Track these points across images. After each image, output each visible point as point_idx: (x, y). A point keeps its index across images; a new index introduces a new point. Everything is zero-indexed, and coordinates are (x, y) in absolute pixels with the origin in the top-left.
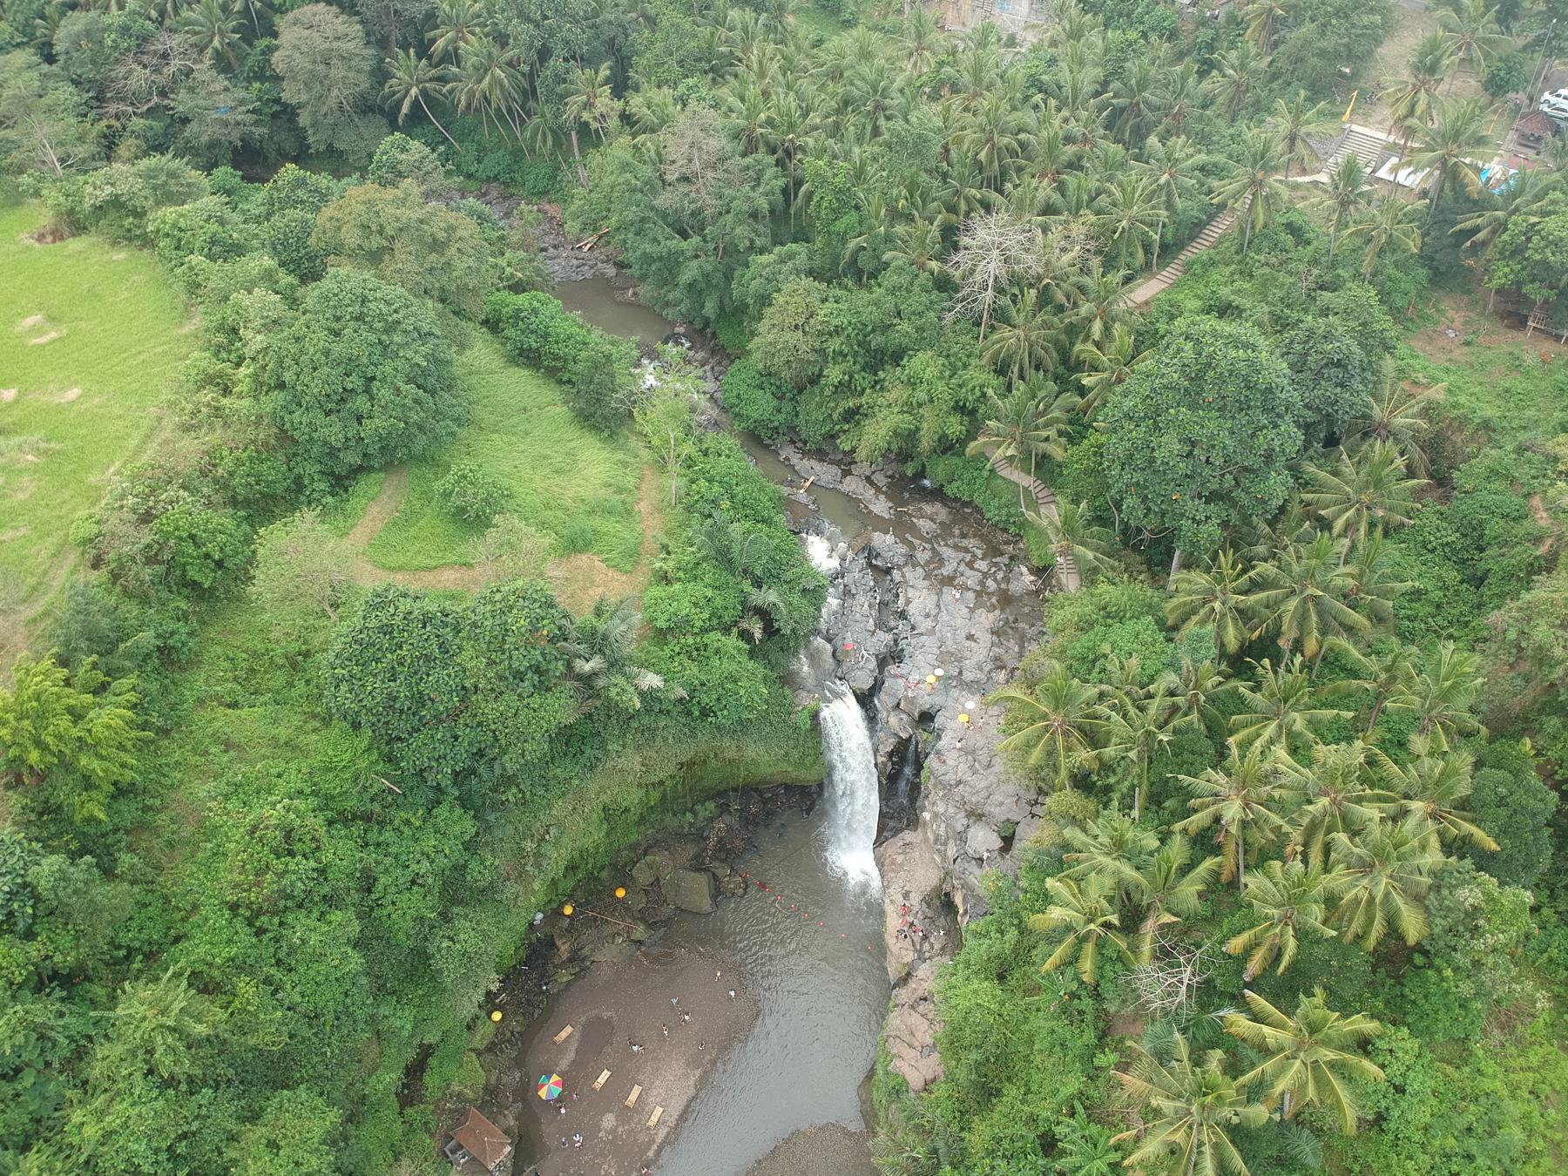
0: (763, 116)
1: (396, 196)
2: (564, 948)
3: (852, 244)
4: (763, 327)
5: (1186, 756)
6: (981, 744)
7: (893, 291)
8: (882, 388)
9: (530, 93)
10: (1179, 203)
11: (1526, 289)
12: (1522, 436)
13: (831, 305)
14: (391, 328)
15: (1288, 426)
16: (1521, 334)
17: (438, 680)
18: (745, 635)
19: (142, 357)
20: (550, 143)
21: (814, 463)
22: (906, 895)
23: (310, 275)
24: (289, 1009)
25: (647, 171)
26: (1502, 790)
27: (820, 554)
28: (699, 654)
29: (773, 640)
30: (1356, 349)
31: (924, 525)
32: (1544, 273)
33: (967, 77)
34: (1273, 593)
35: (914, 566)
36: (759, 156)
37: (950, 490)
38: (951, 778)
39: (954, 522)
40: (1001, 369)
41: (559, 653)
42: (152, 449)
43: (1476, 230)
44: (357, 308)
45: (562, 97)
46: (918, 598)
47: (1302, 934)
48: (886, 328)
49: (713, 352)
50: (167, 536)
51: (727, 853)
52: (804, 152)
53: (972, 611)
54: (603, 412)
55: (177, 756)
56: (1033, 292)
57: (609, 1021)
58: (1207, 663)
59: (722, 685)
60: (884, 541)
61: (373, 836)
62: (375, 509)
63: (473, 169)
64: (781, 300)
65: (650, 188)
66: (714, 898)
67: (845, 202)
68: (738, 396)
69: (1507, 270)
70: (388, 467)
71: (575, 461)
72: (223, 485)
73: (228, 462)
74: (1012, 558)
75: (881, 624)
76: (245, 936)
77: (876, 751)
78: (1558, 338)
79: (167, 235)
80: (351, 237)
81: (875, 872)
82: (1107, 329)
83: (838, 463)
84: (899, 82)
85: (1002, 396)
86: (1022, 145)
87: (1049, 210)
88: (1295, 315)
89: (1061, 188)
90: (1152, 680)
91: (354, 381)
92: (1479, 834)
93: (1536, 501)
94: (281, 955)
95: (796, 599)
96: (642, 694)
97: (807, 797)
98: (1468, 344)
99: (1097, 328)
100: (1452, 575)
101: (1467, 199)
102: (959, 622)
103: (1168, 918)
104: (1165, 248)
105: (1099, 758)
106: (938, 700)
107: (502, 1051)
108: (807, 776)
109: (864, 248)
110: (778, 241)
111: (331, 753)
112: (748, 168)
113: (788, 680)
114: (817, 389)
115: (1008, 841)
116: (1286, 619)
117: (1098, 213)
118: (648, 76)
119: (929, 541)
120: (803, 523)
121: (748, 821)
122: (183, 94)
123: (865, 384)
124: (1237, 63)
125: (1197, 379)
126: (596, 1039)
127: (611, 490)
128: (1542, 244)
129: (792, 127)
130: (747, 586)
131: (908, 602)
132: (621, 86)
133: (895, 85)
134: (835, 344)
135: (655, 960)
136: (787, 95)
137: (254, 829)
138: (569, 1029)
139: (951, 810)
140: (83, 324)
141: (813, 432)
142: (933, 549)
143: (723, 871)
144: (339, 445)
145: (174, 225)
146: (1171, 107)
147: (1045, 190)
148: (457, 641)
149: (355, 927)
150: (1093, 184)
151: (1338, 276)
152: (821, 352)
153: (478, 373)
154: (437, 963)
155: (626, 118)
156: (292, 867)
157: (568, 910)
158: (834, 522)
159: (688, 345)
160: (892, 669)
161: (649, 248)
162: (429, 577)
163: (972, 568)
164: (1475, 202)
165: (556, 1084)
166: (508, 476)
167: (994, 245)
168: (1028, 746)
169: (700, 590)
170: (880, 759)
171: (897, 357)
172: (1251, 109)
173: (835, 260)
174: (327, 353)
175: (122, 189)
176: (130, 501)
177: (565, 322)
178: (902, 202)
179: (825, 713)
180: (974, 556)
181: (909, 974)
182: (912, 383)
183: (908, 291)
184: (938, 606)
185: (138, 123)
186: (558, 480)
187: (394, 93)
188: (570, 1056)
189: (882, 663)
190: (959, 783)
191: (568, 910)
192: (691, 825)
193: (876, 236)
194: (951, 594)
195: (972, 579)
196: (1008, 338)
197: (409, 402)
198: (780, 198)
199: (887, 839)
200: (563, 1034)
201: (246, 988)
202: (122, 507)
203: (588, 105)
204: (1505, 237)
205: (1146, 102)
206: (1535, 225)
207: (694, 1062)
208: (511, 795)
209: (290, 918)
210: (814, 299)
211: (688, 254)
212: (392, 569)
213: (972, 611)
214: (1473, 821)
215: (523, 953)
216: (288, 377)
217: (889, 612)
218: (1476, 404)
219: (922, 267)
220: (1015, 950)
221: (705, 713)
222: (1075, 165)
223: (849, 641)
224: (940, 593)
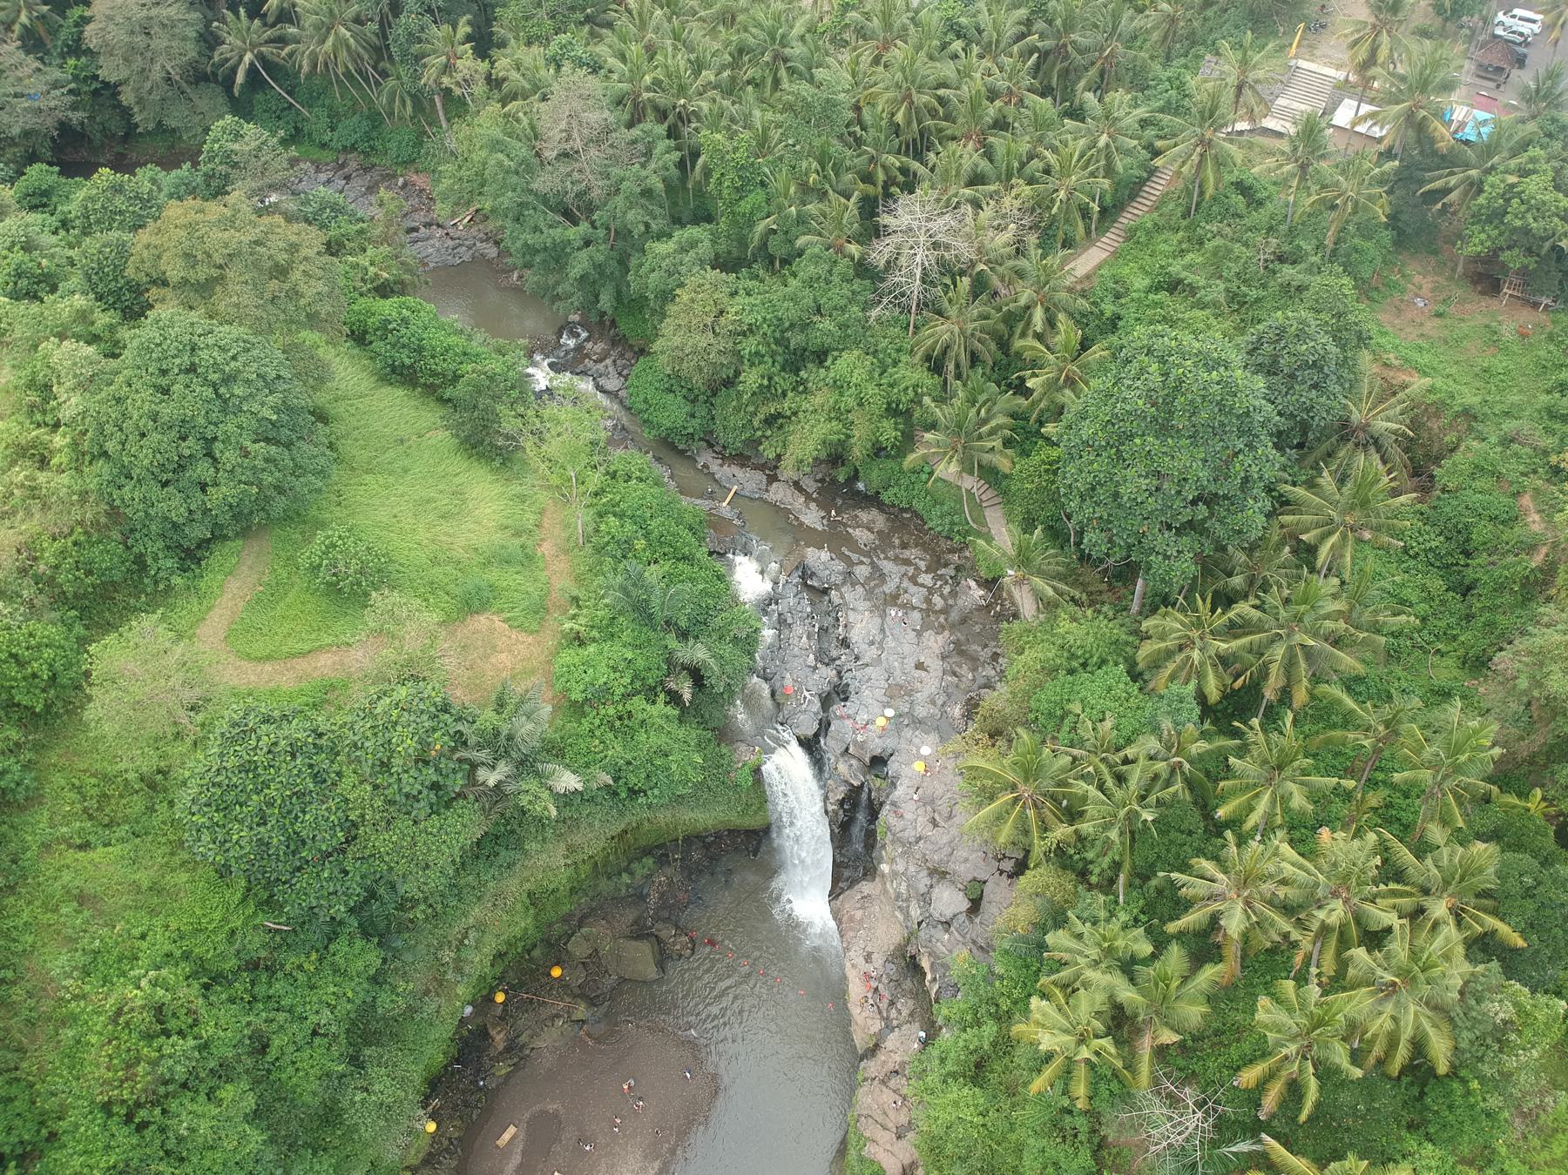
0: (648, 79)
1: (229, 213)
2: (499, 1038)
3: (760, 227)
4: (667, 327)
5: (1173, 835)
6: (939, 792)
7: (810, 283)
9: (380, 51)
10: (1119, 166)
11: (1505, 256)
12: (1509, 426)
13: (741, 299)
14: (229, 379)
15: (1266, 448)
16: (1495, 302)
17: (317, 820)
18: (674, 698)
20: (409, 108)
21: (735, 470)
22: (868, 958)
23: (134, 312)
25: (521, 150)
26: (1528, 880)
28: (624, 725)
29: (702, 701)
30: (1333, 349)
31: (861, 535)
32: (1526, 240)
33: (876, 22)
35: (853, 585)
36: (647, 126)
37: (886, 497)
38: (910, 834)
39: (893, 530)
40: (935, 364)
41: (457, 762)
43: (1447, 191)
44: (186, 359)
45: (418, 58)
46: (861, 624)
47: (1326, 1073)
48: (805, 326)
49: (614, 343)
53: (919, 634)
55: (25, 916)
56: (966, 280)
57: (556, 1116)
58: (1190, 726)
60: (818, 558)
61: (261, 990)
62: (234, 585)
64: (685, 298)
65: (526, 169)
67: (749, 180)
68: (646, 401)
69: (1483, 236)
70: (245, 533)
71: (464, 501)
72: (46, 583)
73: (49, 556)
74: (958, 569)
75: (824, 658)
76: (124, 1137)
77: (826, 798)
78: (1536, 305)
80: (174, 273)
81: (832, 924)
82: (1051, 322)
83: (761, 467)
84: (799, 28)
85: (940, 400)
87: (976, 179)
88: (1254, 293)
89: (989, 155)
91: (191, 446)
92: (1503, 929)
93: (1526, 501)
95: (727, 650)
96: (557, 797)
97: (752, 843)
98: (1439, 315)
99: (1038, 316)
100: (1437, 584)
101: (1435, 153)
102: (907, 649)
103: (1169, 1037)
104: (1104, 211)
105: (1076, 831)
106: (890, 743)
107: (440, 1163)
109: (774, 232)
110: (678, 221)
111: (198, 912)
112: (634, 142)
113: (724, 734)
114: (732, 392)
115: (975, 906)
117: (1031, 181)
118: (515, 30)
120: (723, 542)
125: (1167, 407)
127: (508, 533)
128: (1523, 208)
129: (682, 90)
130: (672, 642)
132: (484, 44)
134: (750, 345)
137: (119, 1013)
138: (512, 1130)
139: (912, 869)
142: (872, 563)
144: (181, 520)
146: (1102, 50)
147: (968, 156)
149: (250, 1102)
150: (1024, 147)
151: (1299, 248)
152: (738, 354)
154: (350, 1118)
155: (494, 82)
156: (167, 1050)
157: (500, 998)
158: (764, 538)
159: (584, 335)
160: (838, 709)
161: (530, 239)
162: (302, 665)
163: (916, 584)
164: (1443, 157)
167: (918, 227)
168: (999, 818)
169: (618, 651)
170: (830, 808)
171: (821, 356)
172: (1186, 43)
173: (743, 242)
174: (155, 417)
177: (442, 324)
180: (917, 568)
181: (877, 1046)
182: (839, 386)
183: (828, 282)
184: (882, 630)
186: (445, 526)
187: (227, 60)
188: (516, 1159)
189: (826, 701)
191: (500, 998)
193: (787, 217)
195: (916, 596)
196: (942, 332)
197: (259, 463)
198: (674, 172)
199: (843, 891)
200: (507, 1136)
203: (447, 69)
204: (1481, 200)
205: (1073, 42)
206: (1513, 186)
207: (651, 1153)
208: (419, 913)
209: (173, 1106)
210: (721, 295)
211: (576, 245)
212: (259, 660)
213: (919, 634)
214: (1494, 913)
215: (454, 1051)
216: (111, 446)
217: (831, 642)
218: (1453, 387)
219: (840, 250)
221: (633, 793)
222: (1001, 125)
223: (788, 682)
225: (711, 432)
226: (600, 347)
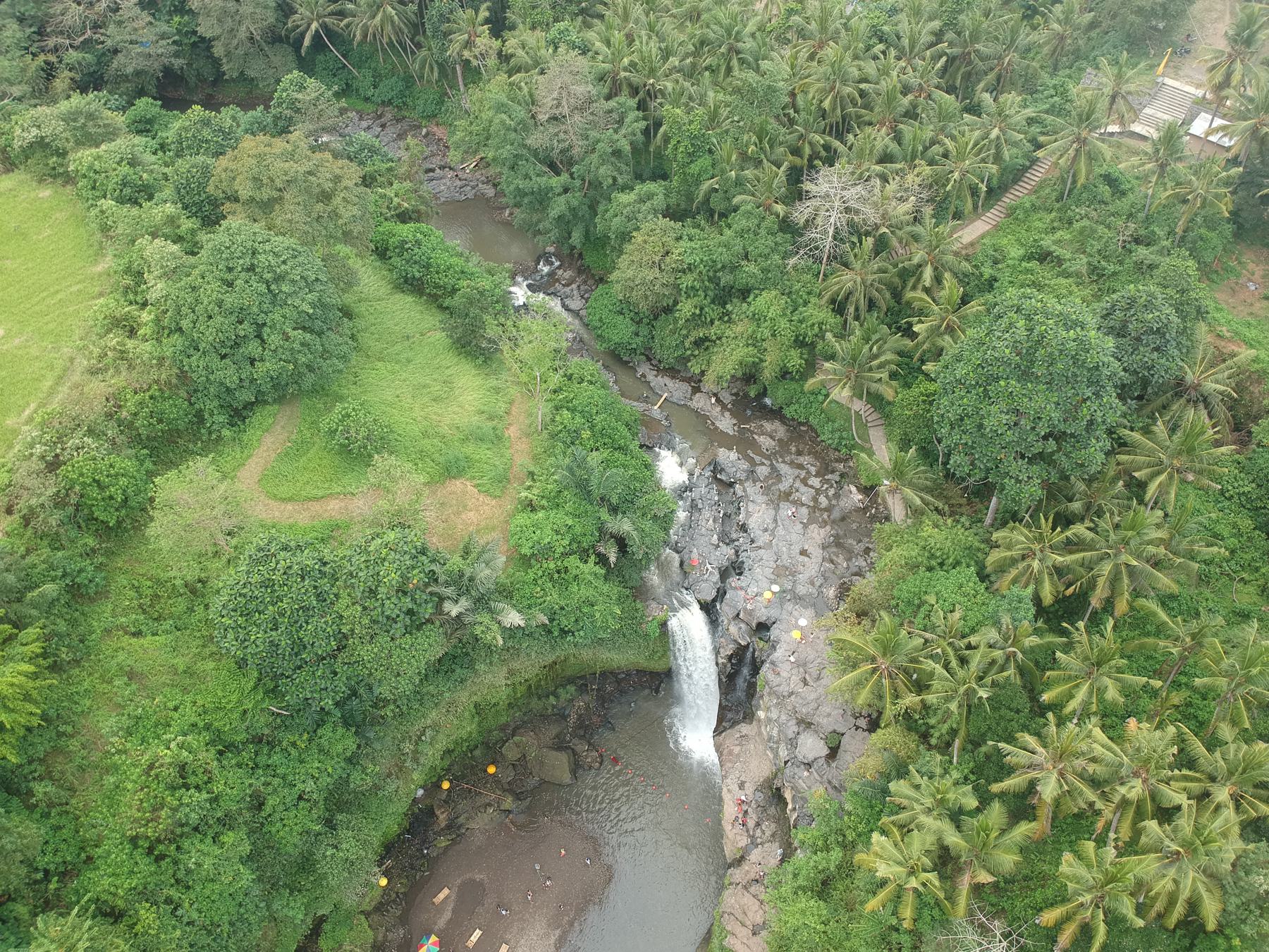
0: (626, 61)
2: (442, 817)
3: (705, 186)
4: (623, 262)
5: (1003, 711)
7: (741, 234)
8: (729, 321)
13: (684, 244)
14: (279, 278)
17: (317, 630)
18: (602, 560)
19: (59, 297)
20: (436, 74)
21: (667, 380)
23: (211, 220)
24: (188, 924)
25: (520, 113)
27: (671, 469)
28: (561, 578)
29: (624, 564)
30: (1175, 319)
31: (765, 442)
33: (814, 26)
34: (1088, 554)
36: (622, 99)
37: (788, 412)
38: (784, 689)
39: (791, 440)
40: (838, 306)
41: (429, 594)
42: (64, 390)
44: (247, 261)
45: (446, 34)
46: (757, 513)
48: (734, 268)
49: (580, 271)
50: (73, 483)
51: (585, 729)
52: (664, 96)
53: (805, 526)
54: (473, 345)
56: (870, 240)
57: (481, 884)
58: (1026, 623)
59: (579, 608)
60: (728, 457)
61: (262, 760)
62: (269, 440)
63: (370, 94)
64: (640, 239)
66: (574, 773)
67: (700, 147)
68: (600, 320)
70: (280, 400)
72: (127, 426)
74: (842, 476)
75: (725, 539)
76: (145, 865)
77: (717, 652)
79: (84, 176)
82: (938, 279)
83: (688, 380)
84: (751, 27)
85: (840, 337)
86: (862, 94)
87: (886, 158)
88: (1111, 268)
89: (898, 139)
90: (973, 631)
91: (246, 329)
94: (181, 875)
95: (647, 525)
96: (504, 629)
97: (658, 681)
99: (928, 273)
102: (794, 537)
104: (990, 191)
106: (774, 613)
107: (388, 911)
108: (658, 666)
109: (716, 191)
110: (639, 177)
112: (610, 111)
113: (640, 592)
114: (670, 317)
115: (833, 753)
116: (1101, 582)
117: (931, 163)
119: (768, 458)
120: (653, 437)
121: (603, 699)
122: (112, 29)
123: (714, 315)
124: (1062, 17)
126: (470, 898)
129: (652, 72)
130: (604, 515)
131: (748, 514)
132: (498, 26)
133: (748, 30)
134: (687, 281)
135: (520, 827)
136: (650, 38)
137: (151, 767)
138: (446, 891)
139: (784, 717)
140: (8, 263)
141: (670, 358)
142: (772, 465)
143: (582, 747)
144: (233, 386)
145: (90, 168)
147: (881, 138)
148: (335, 590)
149: (246, 848)
150: (928, 134)
153: (366, 300)
154: (322, 868)
155: (504, 57)
156: (186, 800)
157: (446, 785)
158: (685, 437)
159: (557, 264)
160: (733, 581)
161: (522, 184)
163: (806, 485)
165: (434, 944)
166: (390, 405)
167: (834, 194)
168: (859, 684)
169: (562, 518)
170: (721, 661)
171: (745, 293)
173: (690, 198)
174: (220, 304)
175: (46, 131)
176: (39, 449)
177: (446, 246)
178: (753, 147)
179: (673, 624)
180: (808, 472)
182: (757, 318)
183: (756, 234)
184: (775, 521)
185: (73, 56)
187: (298, 27)
188: (448, 915)
189: (724, 574)
190: (792, 693)
191: (446, 785)
192: (554, 707)
193: (728, 179)
194: (787, 510)
195: (805, 495)
196: (846, 280)
197: (296, 346)
200: (441, 896)
201: (147, 915)
202: (32, 455)
203: (468, 44)
205: (976, 51)
207: (554, 923)
208: (388, 711)
210: (669, 240)
211: (557, 191)
212: (283, 500)
213: (805, 526)
216: (185, 324)
217: (732, 527)
219: (768, 208)
220: (839, 867)
221: (564, 633)
222: (911, 114)
223: (695, 555)
224: (777, 508)
225: (651, 349)
226: (568, 274)
